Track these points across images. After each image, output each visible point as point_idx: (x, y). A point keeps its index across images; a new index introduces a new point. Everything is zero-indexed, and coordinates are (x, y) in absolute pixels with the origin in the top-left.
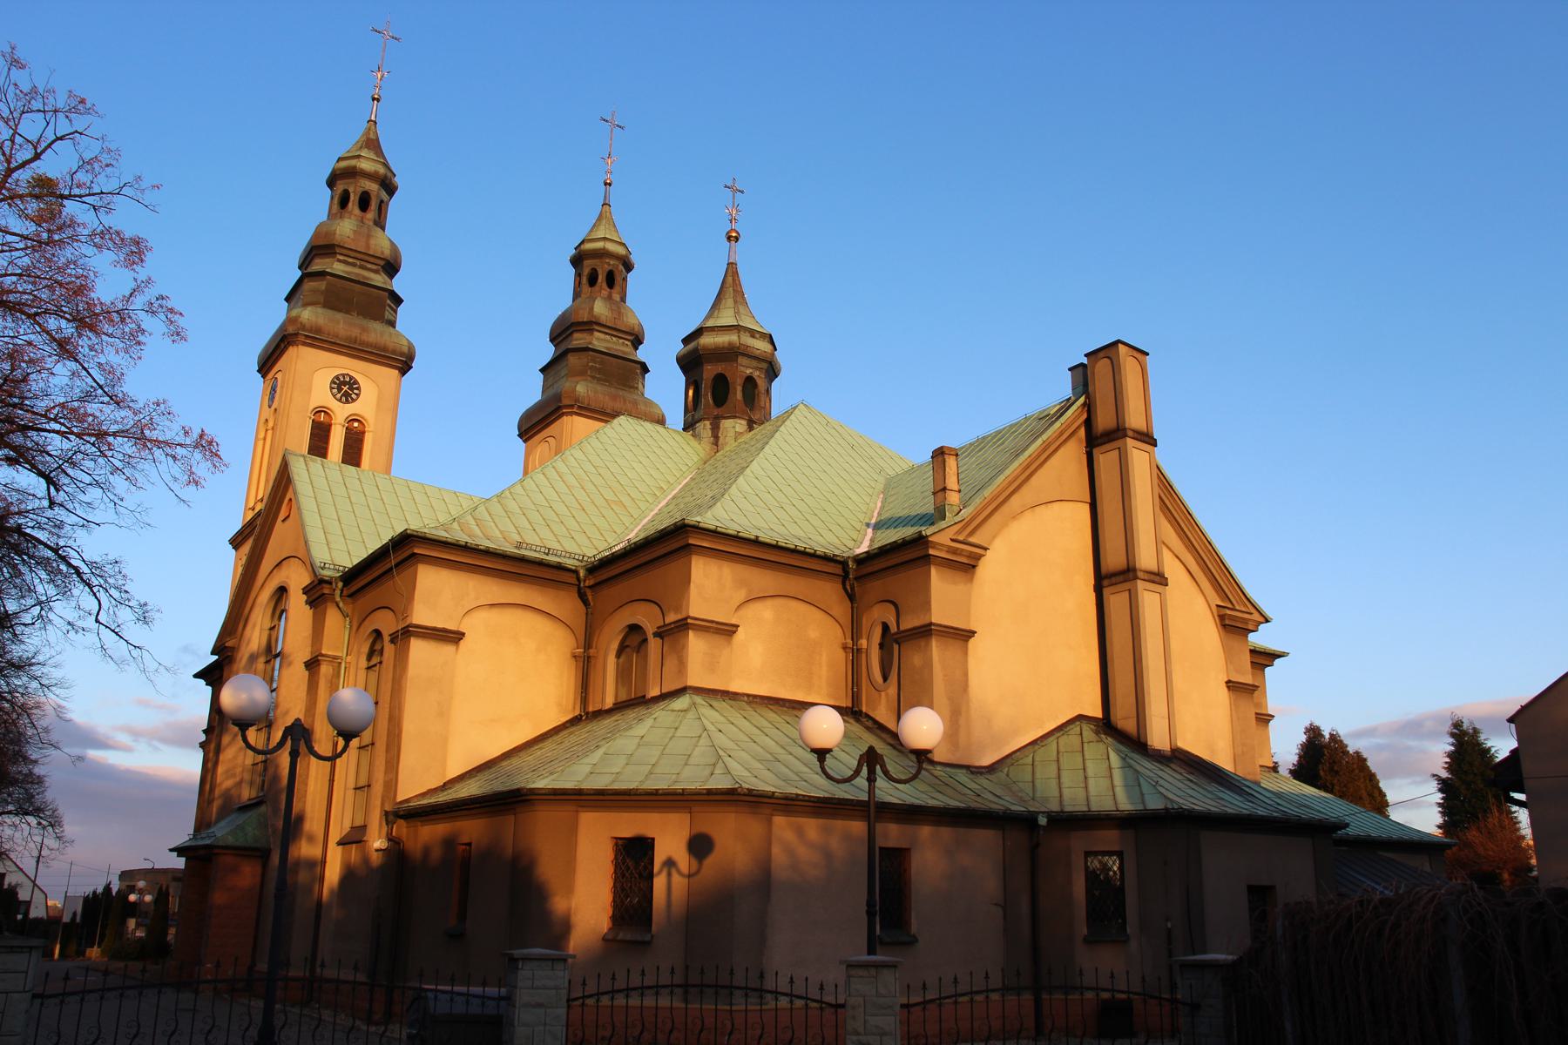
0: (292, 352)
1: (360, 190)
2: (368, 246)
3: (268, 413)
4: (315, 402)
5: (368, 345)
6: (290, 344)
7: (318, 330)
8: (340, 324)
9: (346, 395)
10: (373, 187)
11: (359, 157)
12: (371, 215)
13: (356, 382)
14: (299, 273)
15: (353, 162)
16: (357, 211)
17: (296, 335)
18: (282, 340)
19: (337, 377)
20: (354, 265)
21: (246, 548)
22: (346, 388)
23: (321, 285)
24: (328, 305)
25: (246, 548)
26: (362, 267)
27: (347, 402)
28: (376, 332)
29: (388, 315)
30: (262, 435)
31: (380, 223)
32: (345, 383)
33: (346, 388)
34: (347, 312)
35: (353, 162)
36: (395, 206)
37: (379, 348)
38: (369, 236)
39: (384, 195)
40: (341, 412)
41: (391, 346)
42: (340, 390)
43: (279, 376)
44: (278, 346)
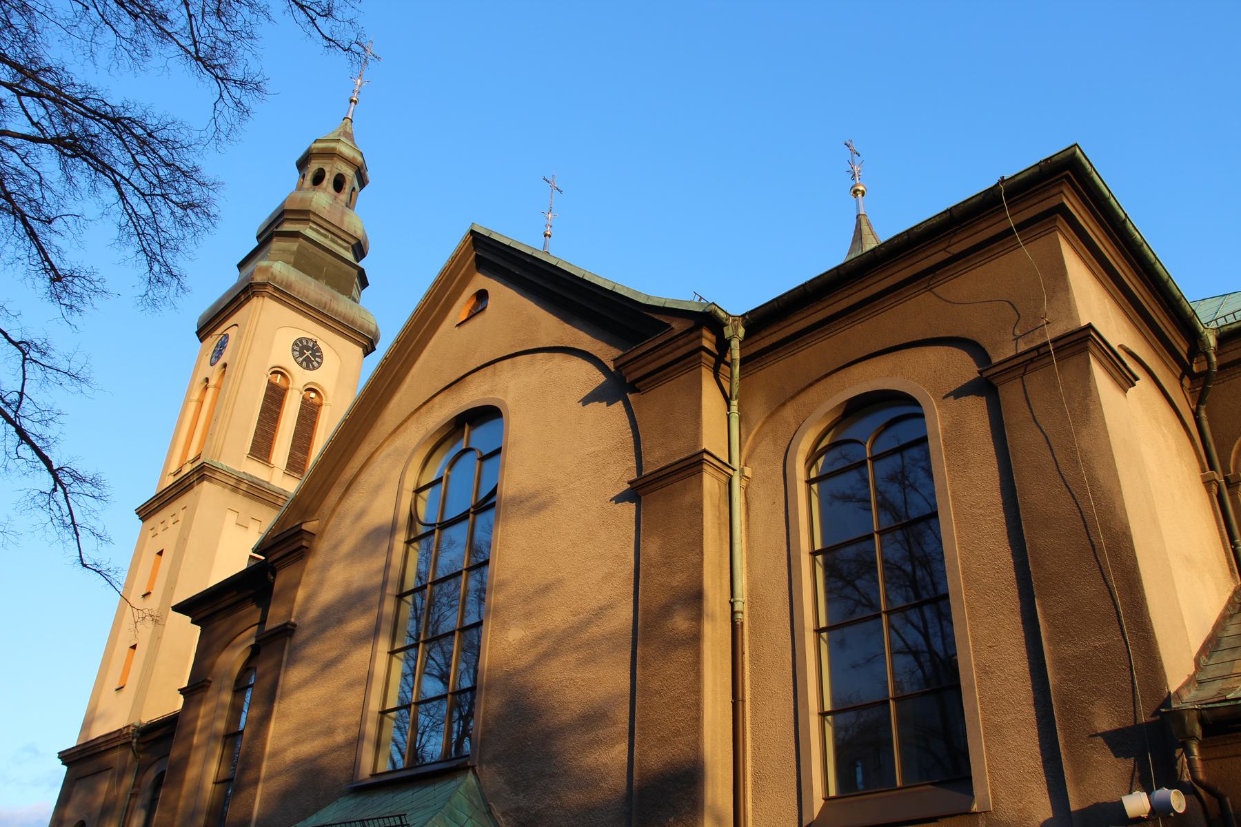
0: (256, 303)
1: (336, 172)
2: (342, 221)
3: (214, 373)
4: (275, 361)
5: (336, 313)
6: (254, 294)
7: (289, 286)
8: (312, 289)
9: (308, 360)
10: (349, 173)
11: (338, 141)
12: (344, 196)
13: (319, 350)
14: (256, 244)
15: (333, 145)
16: (331, 189)
17: (265, 284)
18: (245, 290)
19: (300, 340)
20: (326, 237)
21: (491, 501)
22: (308, 354)
23: (293, 245)
24: (297, 265)
25: (491, 501)
26: (332, 240)
27: (308, 368)
28: (342, 305)
29: (354, 292)
30: (196, 395)
31: (350, 204)
32: (308, 349)
33: (308, 354)
34: (316, 278)
35: (333, 145)
36: (363, 196)
37: (348, 321)
38: (343, 214)
39: (357, 188)
40: (300, 378)
41: (359, 321)
42: (302, 354)
43: (232, 333)
44: (237, 298)
